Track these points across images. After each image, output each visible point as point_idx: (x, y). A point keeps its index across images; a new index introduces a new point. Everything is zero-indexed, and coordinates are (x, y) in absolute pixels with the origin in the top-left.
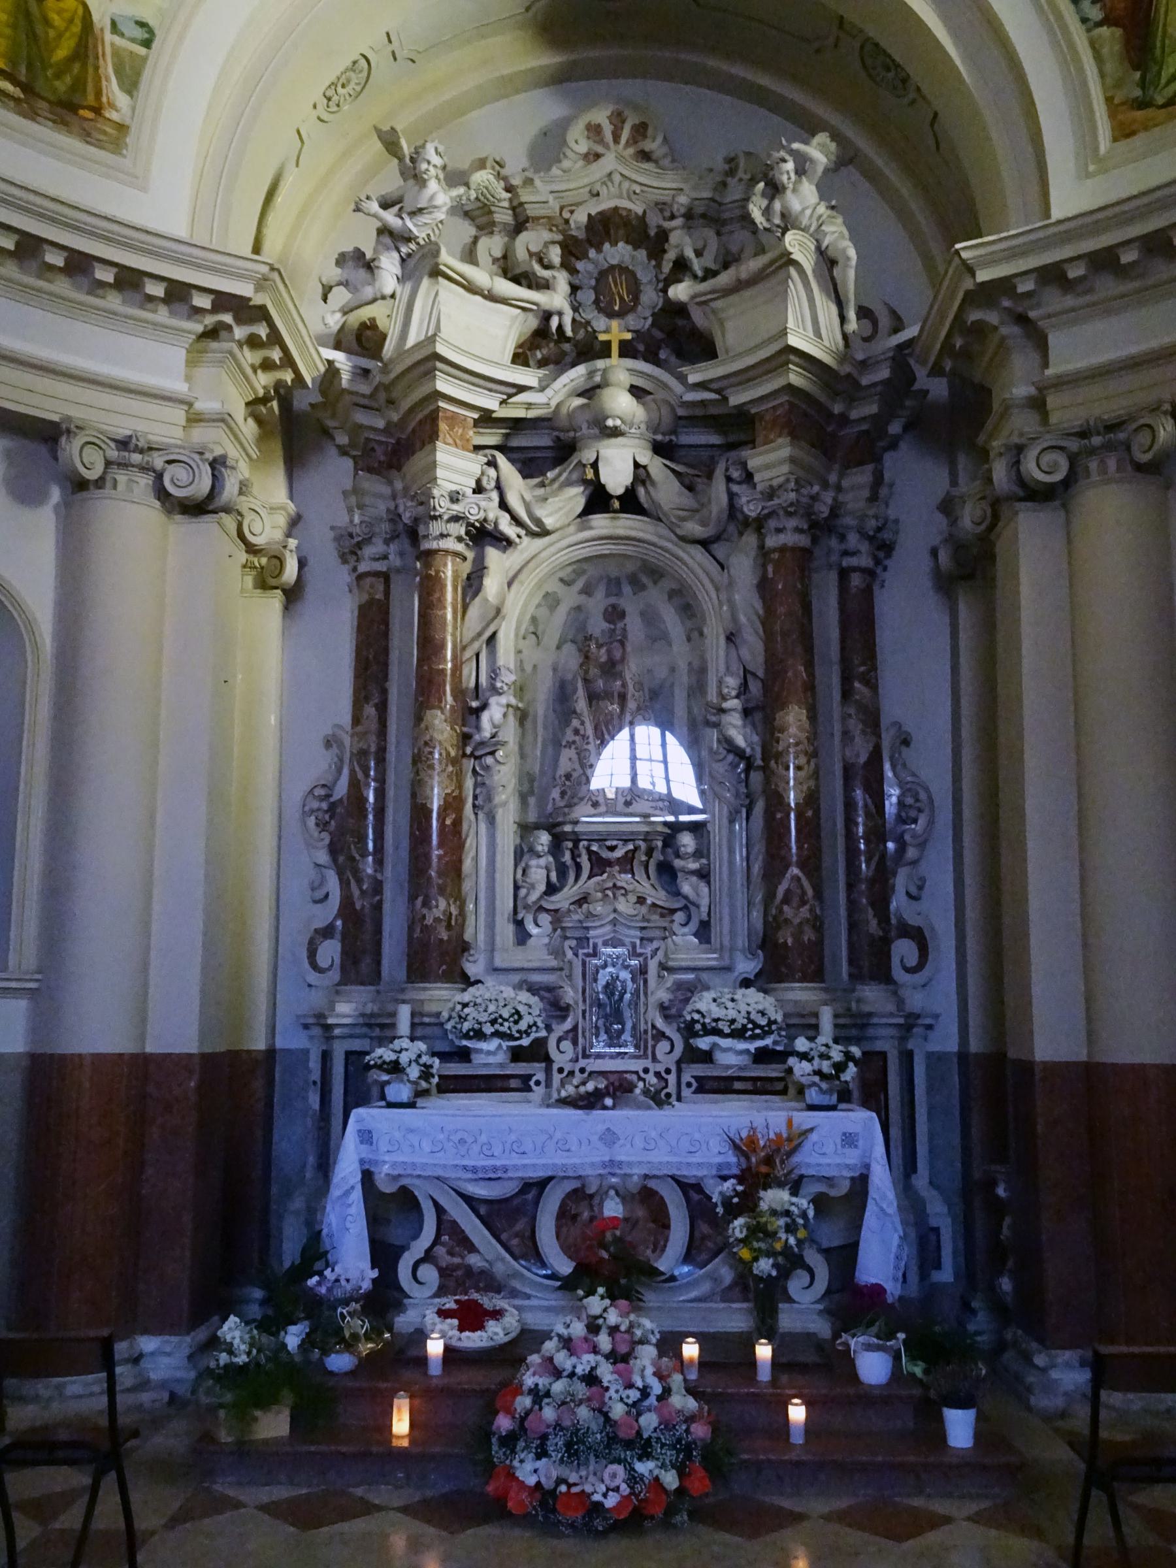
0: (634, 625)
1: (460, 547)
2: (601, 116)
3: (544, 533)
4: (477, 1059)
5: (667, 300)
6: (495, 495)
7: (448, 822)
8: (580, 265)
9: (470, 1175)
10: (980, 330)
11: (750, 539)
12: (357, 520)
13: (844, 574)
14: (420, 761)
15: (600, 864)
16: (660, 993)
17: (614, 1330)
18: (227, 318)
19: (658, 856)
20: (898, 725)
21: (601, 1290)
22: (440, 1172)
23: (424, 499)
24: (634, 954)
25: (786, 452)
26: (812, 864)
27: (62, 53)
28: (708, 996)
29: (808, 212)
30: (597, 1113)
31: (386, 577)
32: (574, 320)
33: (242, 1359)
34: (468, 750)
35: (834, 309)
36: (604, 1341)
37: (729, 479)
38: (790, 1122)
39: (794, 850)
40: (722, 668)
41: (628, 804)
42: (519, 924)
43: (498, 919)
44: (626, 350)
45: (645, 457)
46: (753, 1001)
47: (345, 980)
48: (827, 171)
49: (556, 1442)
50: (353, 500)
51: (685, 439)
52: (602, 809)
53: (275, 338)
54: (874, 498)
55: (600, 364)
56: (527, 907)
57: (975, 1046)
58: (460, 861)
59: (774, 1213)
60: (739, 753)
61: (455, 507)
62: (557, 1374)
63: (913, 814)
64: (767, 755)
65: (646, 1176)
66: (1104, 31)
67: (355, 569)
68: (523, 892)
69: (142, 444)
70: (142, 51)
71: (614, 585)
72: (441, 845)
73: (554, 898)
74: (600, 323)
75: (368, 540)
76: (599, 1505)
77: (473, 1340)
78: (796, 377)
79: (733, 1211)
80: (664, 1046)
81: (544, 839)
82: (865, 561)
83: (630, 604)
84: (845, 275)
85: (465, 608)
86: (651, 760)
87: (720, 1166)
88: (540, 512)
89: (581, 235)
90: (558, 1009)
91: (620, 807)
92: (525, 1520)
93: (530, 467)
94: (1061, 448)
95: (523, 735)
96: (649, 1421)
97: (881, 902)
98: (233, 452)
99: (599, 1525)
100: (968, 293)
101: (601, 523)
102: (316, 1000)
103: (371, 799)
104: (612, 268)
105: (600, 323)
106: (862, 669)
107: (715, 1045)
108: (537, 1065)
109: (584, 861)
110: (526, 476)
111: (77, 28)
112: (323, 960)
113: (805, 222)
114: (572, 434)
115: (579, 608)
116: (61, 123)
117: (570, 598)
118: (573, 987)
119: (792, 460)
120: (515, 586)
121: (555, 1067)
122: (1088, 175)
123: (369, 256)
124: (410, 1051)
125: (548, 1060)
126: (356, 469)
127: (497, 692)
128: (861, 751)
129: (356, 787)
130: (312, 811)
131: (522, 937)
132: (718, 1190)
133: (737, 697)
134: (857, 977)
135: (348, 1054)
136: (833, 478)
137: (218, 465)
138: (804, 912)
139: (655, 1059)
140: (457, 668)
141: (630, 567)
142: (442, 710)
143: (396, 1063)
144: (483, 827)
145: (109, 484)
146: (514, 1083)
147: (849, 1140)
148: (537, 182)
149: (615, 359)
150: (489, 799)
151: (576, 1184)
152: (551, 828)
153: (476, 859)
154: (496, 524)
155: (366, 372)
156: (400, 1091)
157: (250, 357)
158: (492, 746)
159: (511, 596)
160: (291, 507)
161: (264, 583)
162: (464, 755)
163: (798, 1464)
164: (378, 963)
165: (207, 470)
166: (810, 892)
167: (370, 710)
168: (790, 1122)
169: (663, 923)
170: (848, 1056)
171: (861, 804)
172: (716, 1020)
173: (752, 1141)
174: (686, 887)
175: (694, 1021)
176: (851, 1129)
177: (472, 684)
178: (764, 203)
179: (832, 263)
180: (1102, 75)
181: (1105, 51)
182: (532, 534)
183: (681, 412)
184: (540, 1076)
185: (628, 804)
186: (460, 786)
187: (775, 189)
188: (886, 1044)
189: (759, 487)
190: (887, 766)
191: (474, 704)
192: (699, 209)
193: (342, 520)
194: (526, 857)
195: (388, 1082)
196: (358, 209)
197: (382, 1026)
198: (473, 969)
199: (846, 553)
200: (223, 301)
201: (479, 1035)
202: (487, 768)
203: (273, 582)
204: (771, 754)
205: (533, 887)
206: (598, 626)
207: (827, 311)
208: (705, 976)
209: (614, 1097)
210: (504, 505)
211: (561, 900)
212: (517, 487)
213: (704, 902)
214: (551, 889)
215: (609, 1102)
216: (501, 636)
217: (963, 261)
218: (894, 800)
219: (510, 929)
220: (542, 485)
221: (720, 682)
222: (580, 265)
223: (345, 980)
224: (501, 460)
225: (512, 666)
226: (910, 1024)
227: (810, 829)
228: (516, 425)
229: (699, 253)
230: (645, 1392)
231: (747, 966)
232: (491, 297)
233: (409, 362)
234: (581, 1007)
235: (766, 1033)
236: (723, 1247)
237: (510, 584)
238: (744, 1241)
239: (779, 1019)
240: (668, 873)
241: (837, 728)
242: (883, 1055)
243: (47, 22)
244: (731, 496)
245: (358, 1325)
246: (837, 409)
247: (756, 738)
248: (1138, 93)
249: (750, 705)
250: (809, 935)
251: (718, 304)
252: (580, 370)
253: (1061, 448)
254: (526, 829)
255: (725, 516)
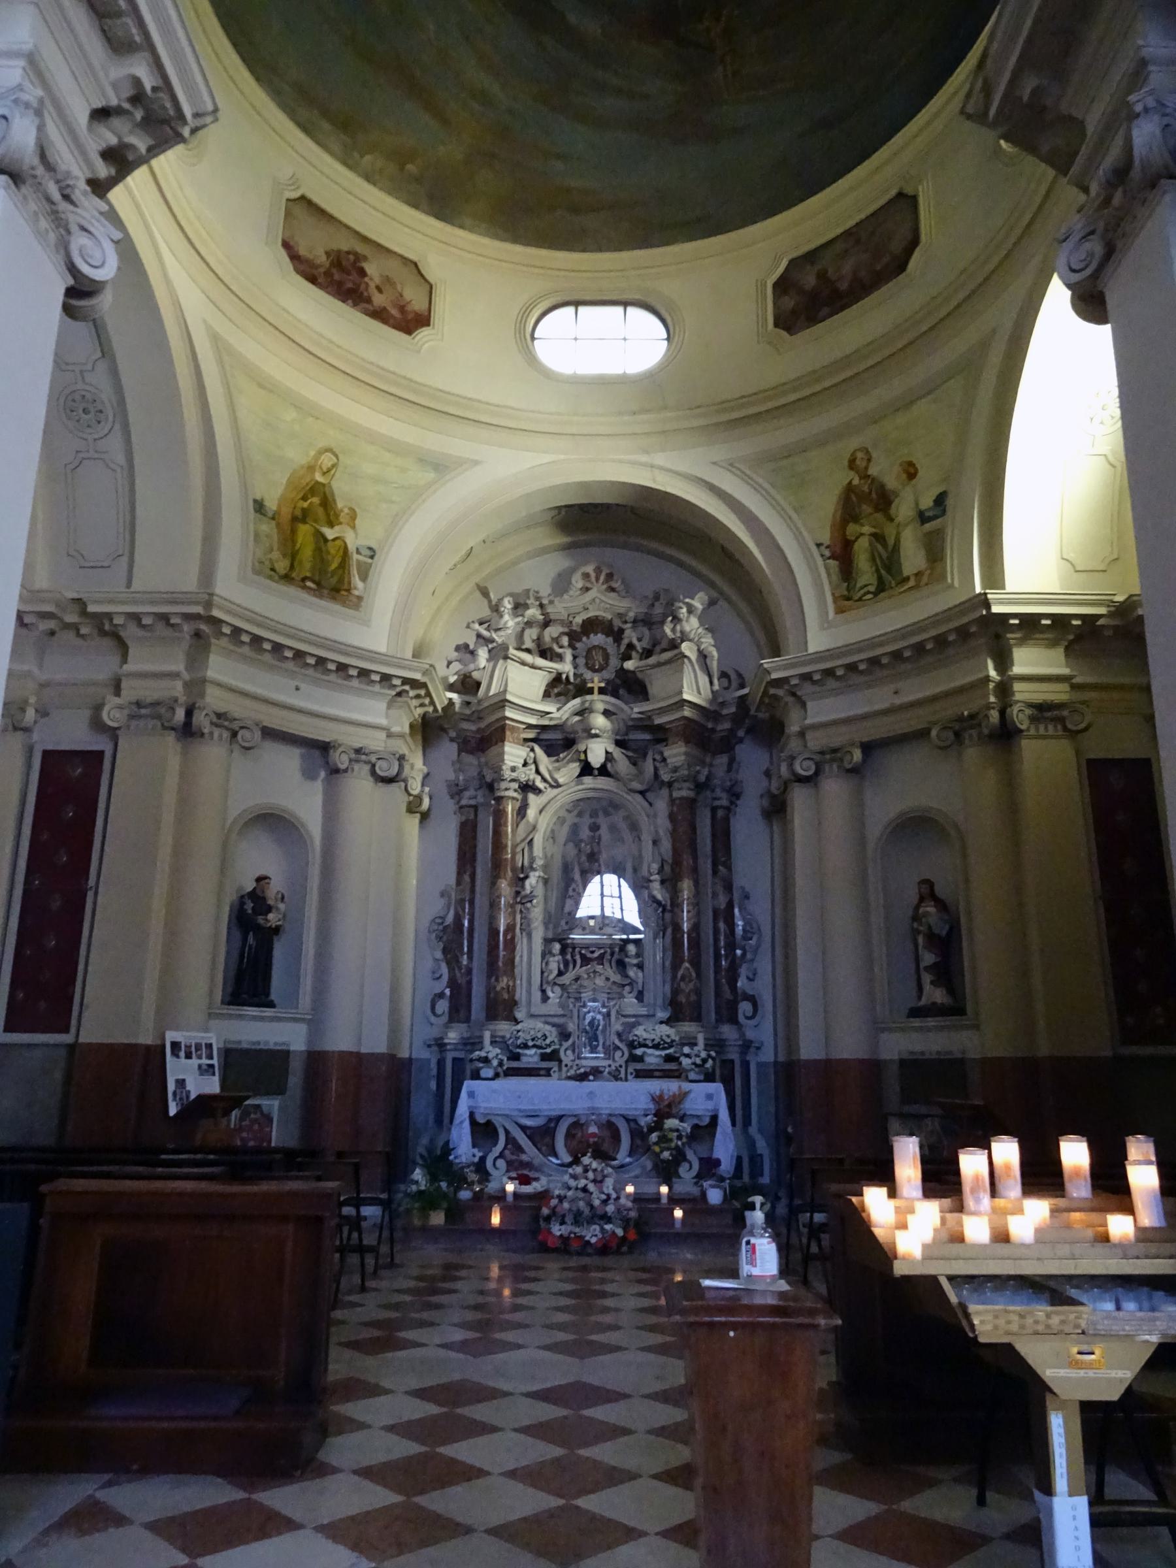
0: (604, 832)
1: (515, 795)
2: (590, 569)
3: (558, 786)
4: (524, 1059)
5: (622, 668)
6: (533, 767)
7: (509, 937)
8: (578, 645)
9: (521, 1114)
10: (775, 697)
11: (665, 792)
12: (461, 778)
13: (714, 810)
14: (493, 905)
15: (586, 961)
16: (617, 1026)
17: (595, 1170)
18: (407, 688)
19: (616, 956)
20: (743, 888)
21: (589, 1154)
22: (507, 1112)
23: (498, 770)
24: (604, 1006)
25: (683, 749)
26: (696, 963)
27: (334, 566)
28: (641, 1028)
29: (693, 632)
30: (585, 1083)
31: (475, 808)
32: (575, 674)
33: (423, 1188)
34: (518, 900)
35: (707, 679)
36: (591, 1175)
37: (654, 760)
38: (680, 1087)
39: (686, 954)
40: (650, 859)
41: (601, 929)
42: (543, 991)
43: (533, 988)
44: (602, 691)
45: (611, 748)
46: (665, 1030)
47: (451, 1020)
48: (702, 612)
49: (569, 1219)
50: (457, 766)
51: (632, 736)
52: (587, 931)
53: (428, 694)
54: (729, 770)
55: (588, 697)
56: (548, 983)
57: (781, 1059)
58: (514, 958)
59: (671, 1130)
60: (659, 903)
61: (513, 774)
62: (569, 1189)
63: (749, 935)
64: (672, 904)
65: (610, 1115)
66: (831, 562)
67: (458, 802)
68: (546, 974)
69: (367, 751)
70: (370, 561)
71: (594, 814)
72: (505, 949)
73: (561, 978)
74: (588, 675)
75: (466, 789)
76: (588, 1242)
77: (527, 1189)
78: (687, 712)
79: (651, 1130)
80: (618, 1054)
81: (557, 947)
82: (725, 802)
83: (603, 821)
84: (712, 663)
85: (517, 826)
86: (612, 896)
87: (645, 1110)
88: (557, 776)
89: (579, 630)
90: (565, 1035)
91: (597, 930)
92: (555, 1250)
93: (551, 750)
94: (812, 759)
95: (546, 890)
96: (610, 1208)
97: (733, 981)
98: (404, 750)
99: (590, 1251)
100: (768, 683)
101: (588, 781)
102: (435, 1032)
103: (466, 924)
104: (595, 647)
105: (588, 675)
106: (723, 859)
107: (644, 1053)
108: (554, 1063)
109: (578, 958)
110: (549, 755)
111: (341, 553)
112: (439, 1010)
113: (692, 636)
114: (572, 736)
115: (575, 824)
116: (334, 599)
117: (571, 819)
118: (574, 1023)
119: (686, 754)
120: (543, 813)
121: (564, 1064)
122: (824, 629)
123: (471, 647)
124: (493, 1052)
125: (560, 1061)
126: (460, 751)
127: (532, 869)
128: (722, 901)
129: (458, 919)
130: (434, 931)
131: (545, 998)
132: (643, 1122)
133: (658, 874)
134: (720, 1020)
135: (454, 1059)
136: (708, 760)
137: (402, 758)
138: (691, 985)
139: (614, 1060)
140: (514, 854)
141: (604, 803)
142: (506, 879)
143: (486, 1058)
144: (525, 941)
145: (350, 770)
146: (542, 1072)
147: (709, 1097)
148: (556, 602)
149: (595, 696)
150: (529, 925)
151: (575, 1119)
152: (560, 941)
153: (521, 956)
154: (534, 781)
155: (468, 703)
156: (487, 1072)
157: (415, 702)
158: (530, 898)
159: (541, 819)
160: (425, 770)
161: (411, 810)
162: (517, 903)
163: (678, 1235)
164: (470, 1011)
165: (397, 763)
166: (694, 975)
167: (467, 878)
168: (680, 1087)
169: (619, 990)
170: (709, 1056)
171: (722, 930)
172: (645, 1040)
173: (661, 1097)
174: (632, 973)
175: (634, 1041)
176: (710, 1091)
177: (520, 865)
178: (672, 626)
179: (705, 657)
180: (830, 583)
181: (831, 571)
182: (552, 786)
183: (631, 723)
184: (556, 1069)
185: (601, 929)
186: (514, 919)
187: (676, 619)
188: (734, 1055)
189: (670, 766)
190: (736, 911)
191: (522, 876)
192: (641, 617)
193: (451, 776)
194: (547, 956)
195: (482, 1068)
196: (468, 627)
197: (473, 1044)
198: (519, 1015)
199: (715, 799)
200: (406, 681)
201: (526, 1046)
202: (528, 909)
203: (417, 810)
204: (675, 904)
205: (551, 972)
206: (585, 833)
207: (703, 679)
208: (641, 1020)
209: (594, 1075)
210: (538, 772)
211: (566, 979)
212: (545, 762)
213: (640, 981)
214: (560, 974)
215: (591, 1078)
216: (535, 840)
217: (765, 669)
218: (740, 928)
219: (539, 994)
220: (557, 761)
221: (649, 867)
222: (578, 645)
223: (451, 1020)
224: (537, 748)
225: (541, 855)
226: (747, 1046)
227: (695, 943)
228: (544, 728)
229: (639, 640)
230: (609, 1196)
231: (662, 1015)
232: (533, 667)
233: (492, 702)
234: (577, 1033)
235: (671, 1046)
236: (648, 1149)
237: (541, 812)
238: (656, 1144)
239: (677, 1039)
240: (621, 965)
241: (710, 891)
242: (732, 1061)
243: (328, 553)
244: (656, 769)
245: (473, 1177)
246: (710, 725)
247: (667, 895)
248: (846, 593)
249: (665, 878)
250: (693, 998)
251: (648, 672)
252: (578, 701)
253: (812, 759)
254: (547, 941)
255: (652, 777)
